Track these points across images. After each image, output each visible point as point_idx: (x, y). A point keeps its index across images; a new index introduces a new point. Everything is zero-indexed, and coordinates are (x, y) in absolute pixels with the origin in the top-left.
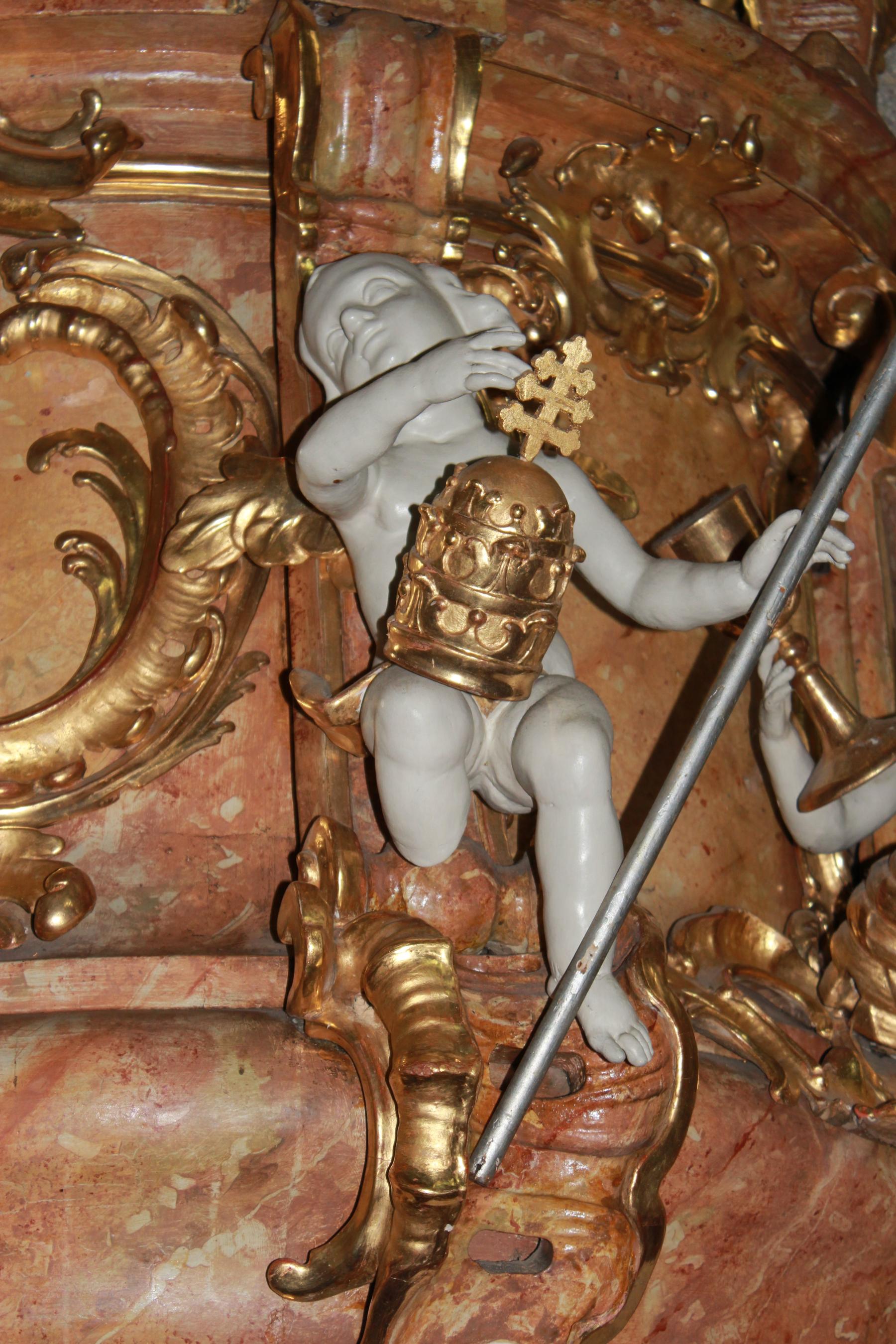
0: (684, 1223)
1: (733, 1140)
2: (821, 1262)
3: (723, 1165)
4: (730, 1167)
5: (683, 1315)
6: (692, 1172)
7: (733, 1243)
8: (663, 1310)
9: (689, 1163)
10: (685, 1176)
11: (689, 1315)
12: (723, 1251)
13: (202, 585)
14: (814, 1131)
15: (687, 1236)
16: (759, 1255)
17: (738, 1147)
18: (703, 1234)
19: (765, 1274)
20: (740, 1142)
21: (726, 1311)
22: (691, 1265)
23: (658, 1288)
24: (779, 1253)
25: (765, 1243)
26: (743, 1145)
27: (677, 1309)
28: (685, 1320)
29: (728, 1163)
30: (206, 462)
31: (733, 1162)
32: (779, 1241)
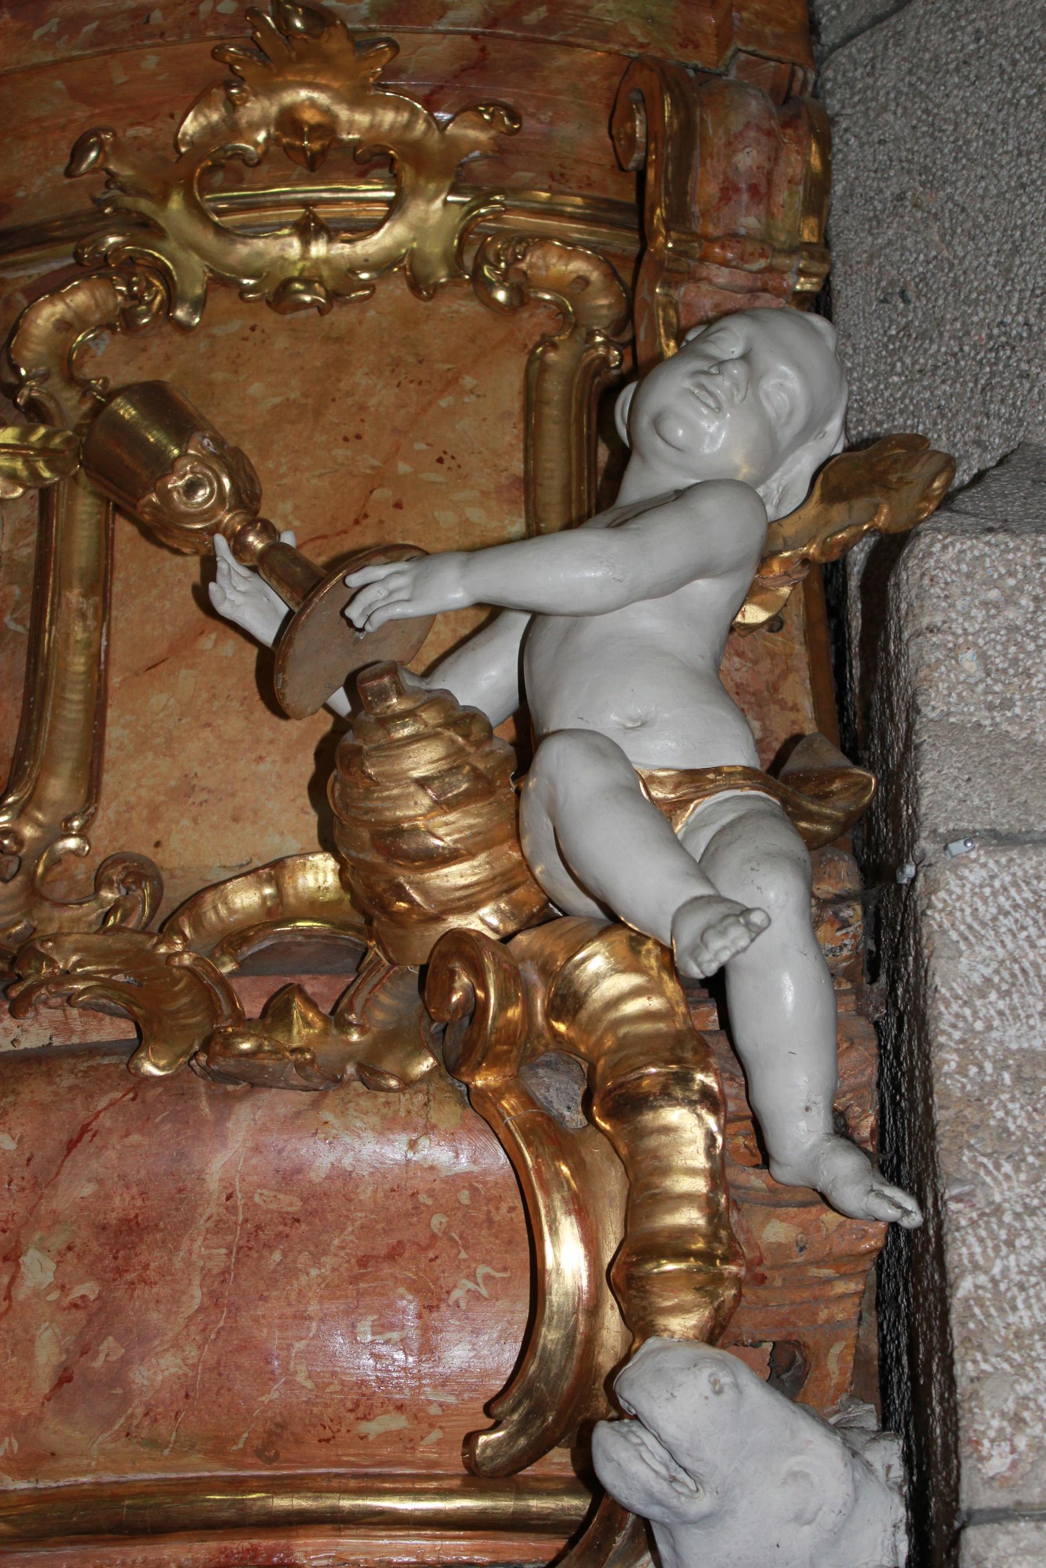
0: (43, 1249)
1: (64, 1137)
2: (285, 1255)
3: (55, 1170)
4: (66, 1170)
5: (94, 1358)
6: (13, 1187)
7: (127, 1259)
8: (64, 1357)
9: (6, 1178)
10: (7, 1195)
11: (102, 1357)
12: (119, 1272)
13: (217, 1063)
14: (204, 1098)
15: (58, 1263)
16: (178, 1264)
17: (72, 1145)
18: (79, 1257)
19: (201, 1286)
20: (75, 1138)
21: (157, 1342)
22: (83, 1297)
23: (49, 1332)
24: (210, 1257)
25: (177, 1249)
26: (80, 1139)
27: (83, 1353)
28: (99, 1363)
29: (61, 1165)
30: (1024, 1313)
31: (68, 1163)
32: (199, 1242)
